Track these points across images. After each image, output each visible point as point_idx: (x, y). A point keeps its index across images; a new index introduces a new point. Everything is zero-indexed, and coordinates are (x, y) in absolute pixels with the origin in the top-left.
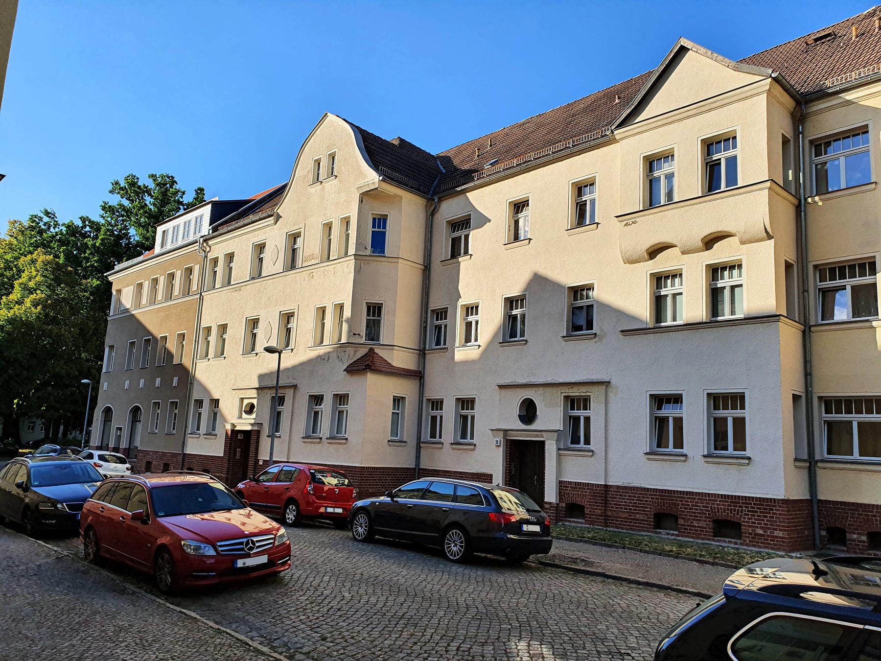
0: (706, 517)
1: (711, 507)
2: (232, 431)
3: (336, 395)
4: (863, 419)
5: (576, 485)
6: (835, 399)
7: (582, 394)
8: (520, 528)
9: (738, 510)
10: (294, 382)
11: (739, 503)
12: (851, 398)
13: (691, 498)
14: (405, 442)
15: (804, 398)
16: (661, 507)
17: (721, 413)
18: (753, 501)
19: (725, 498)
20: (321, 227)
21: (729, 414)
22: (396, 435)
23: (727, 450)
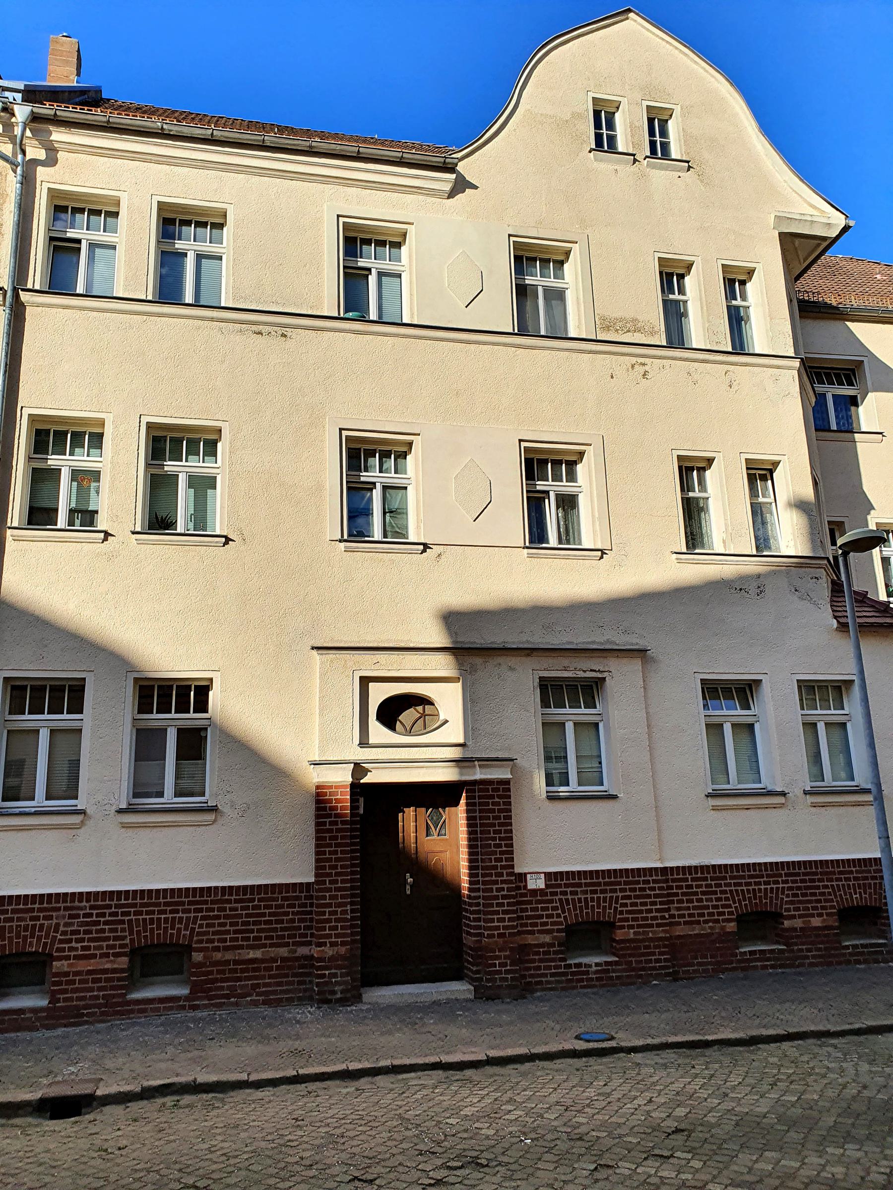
0: (32, 936)
1: (560, 900)
2: (358, 789)
3: (4, 678)
4: (189, 723)
5: (760, 870)
6: (53, 683)
7: (581, 674)
8: (197, 989)
9: (599, 898)
10: (641, 643)
11: (686, 880)
12: (151, 683)
13: (573, 885)
14: (783, 794)
15: (857, 683)
16: (761, 901)
17: (156, 718)
18: (709, 873)
19: (615, 877)
20: (98, 84)
21: (570, 715)
22: (821, 778)
23: (161, 794)
